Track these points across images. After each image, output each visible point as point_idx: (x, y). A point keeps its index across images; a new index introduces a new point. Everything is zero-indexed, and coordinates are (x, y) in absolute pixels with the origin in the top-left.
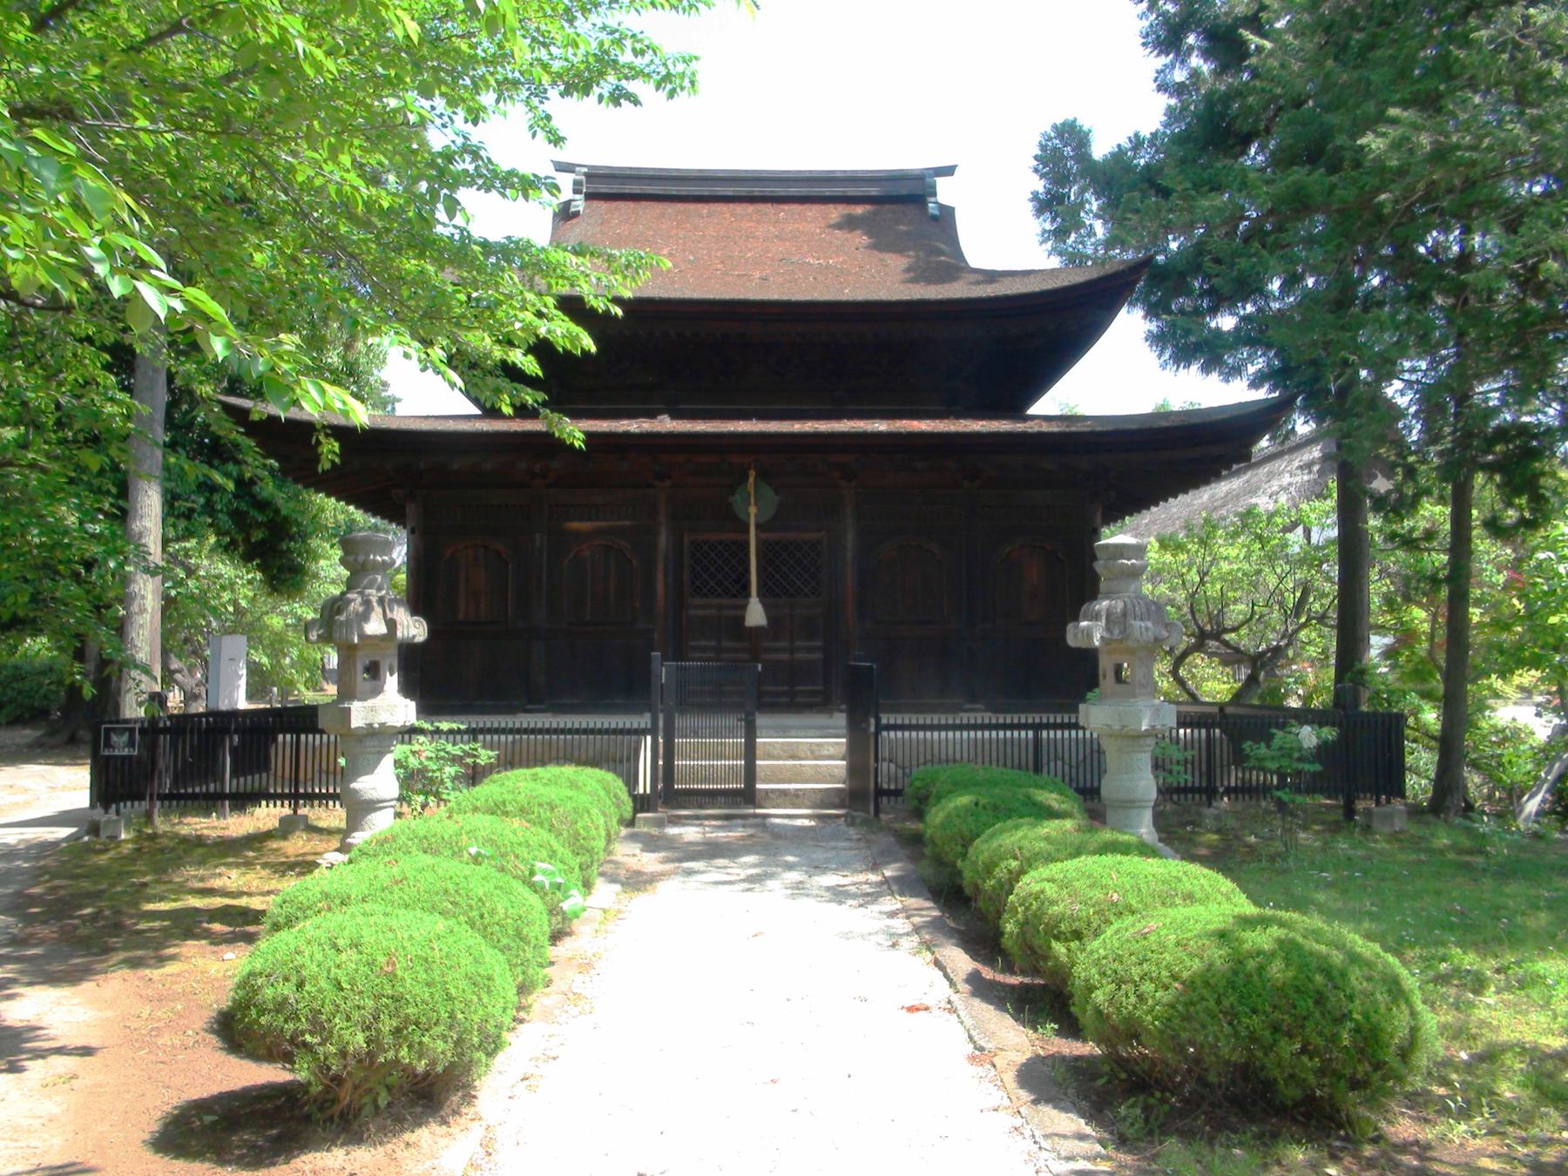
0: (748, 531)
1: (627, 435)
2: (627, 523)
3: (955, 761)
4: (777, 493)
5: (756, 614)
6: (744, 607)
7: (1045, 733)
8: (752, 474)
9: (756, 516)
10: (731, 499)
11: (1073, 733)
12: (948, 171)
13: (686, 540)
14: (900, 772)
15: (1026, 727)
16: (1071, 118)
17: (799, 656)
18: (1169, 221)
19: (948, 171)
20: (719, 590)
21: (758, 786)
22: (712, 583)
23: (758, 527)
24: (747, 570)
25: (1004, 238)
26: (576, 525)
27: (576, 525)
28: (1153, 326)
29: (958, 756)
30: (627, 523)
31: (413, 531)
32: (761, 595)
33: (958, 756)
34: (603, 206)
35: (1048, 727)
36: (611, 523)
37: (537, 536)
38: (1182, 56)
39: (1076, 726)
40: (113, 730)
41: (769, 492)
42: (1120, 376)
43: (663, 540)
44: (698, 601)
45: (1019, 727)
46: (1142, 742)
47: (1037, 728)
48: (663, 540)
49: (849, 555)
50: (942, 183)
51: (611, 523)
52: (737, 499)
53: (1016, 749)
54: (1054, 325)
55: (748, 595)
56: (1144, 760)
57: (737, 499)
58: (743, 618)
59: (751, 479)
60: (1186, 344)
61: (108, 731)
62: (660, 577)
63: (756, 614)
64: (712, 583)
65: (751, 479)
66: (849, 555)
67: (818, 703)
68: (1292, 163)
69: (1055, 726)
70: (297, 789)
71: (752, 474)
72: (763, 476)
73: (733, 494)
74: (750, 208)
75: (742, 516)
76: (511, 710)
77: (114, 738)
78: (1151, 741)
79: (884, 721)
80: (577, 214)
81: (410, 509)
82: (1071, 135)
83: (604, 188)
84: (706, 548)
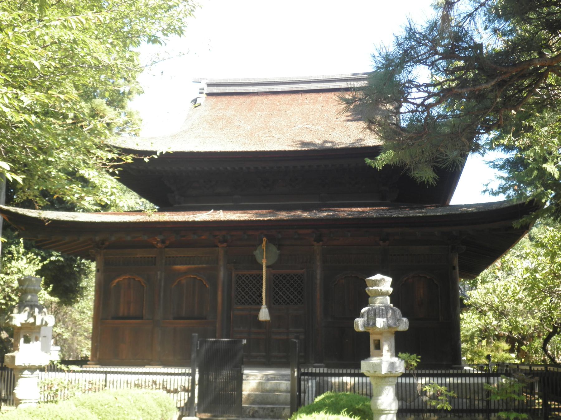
2: (204, 265)
4: (278, 249)
5: (264, 314)
6: (259, 310)
8: (265, 239)
9: (266, 263)
10: (255, 253)
11: (360, 379)
13: (233, 275)
21: (243, 405)
23: (267, 267)
30: (204, 265)
34: (213, 99)
37: (159, 273)
38: (70, 204)
43: (222, 274)
44: (240, 307)
47: (106, 373)
48: (222, 274)
49: (318, 282)
52: (257, 253)
53: (368, 388)
55: (261, 303)
57: (257, 253)
59: (264, 243)
62: (220, 293)
63: (264, 314)
65: (264, 243)
66: (318, 282)
71: (265, 239)
75: (259, 260)
76: (143, 365)
79: (302, 370)
81: (98, 258)
83: (215, 90)
84: (243, 278)
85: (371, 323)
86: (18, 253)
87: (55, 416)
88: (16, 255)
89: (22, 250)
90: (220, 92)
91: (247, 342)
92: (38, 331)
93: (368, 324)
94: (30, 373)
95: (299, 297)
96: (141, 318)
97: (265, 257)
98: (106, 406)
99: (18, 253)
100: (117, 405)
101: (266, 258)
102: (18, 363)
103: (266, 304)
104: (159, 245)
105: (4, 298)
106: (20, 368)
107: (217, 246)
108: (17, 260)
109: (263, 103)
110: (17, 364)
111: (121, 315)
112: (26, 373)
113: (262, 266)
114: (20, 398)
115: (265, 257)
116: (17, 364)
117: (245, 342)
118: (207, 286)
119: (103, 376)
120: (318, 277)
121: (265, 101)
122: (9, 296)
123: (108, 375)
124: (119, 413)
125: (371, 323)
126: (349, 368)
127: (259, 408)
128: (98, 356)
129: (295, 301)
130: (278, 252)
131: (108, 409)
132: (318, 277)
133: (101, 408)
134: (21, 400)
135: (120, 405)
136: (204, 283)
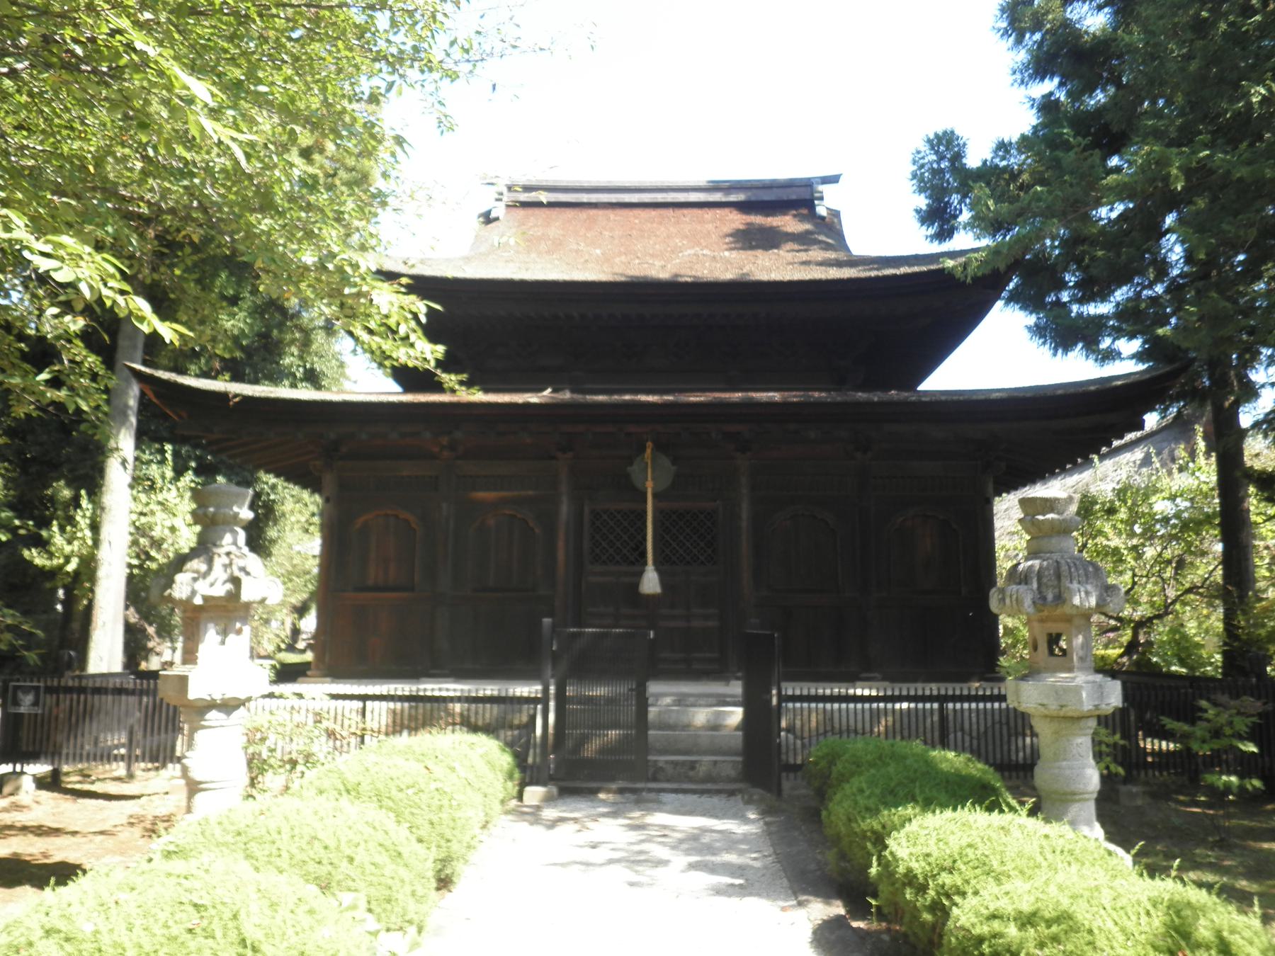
0: (645, 502)
1: (527, 405)
2: (531, 493)
3: (856, 732)
4: (673, 464)
5: (651, 582)
6: (640, 574)
7: (951, 705)
8: (649, 444)
12: (834, 179)
13: (587, 510)
14: (799, 742)
15: (931, 699)
16: (949, 129)
17: (696, 624)
18: (1037, 221)
19: (834, 179)
20: (618, 558)
22: (611, 551)
23: (655, 496)
24: (645, 539)
25: (884, 225)
26: (481, 495)
27: (481, 495)
28: (1032, 319)
29: (860, 726)
30: (531, 493)
31: (327, 500)
32: (657, 563)
33: (860, 726)
34: (521, 212)
35: (954, 699)
36: (516, 493)
37: (444, 505)
39: (1002, 698)
40: (19, 687)
41: (666, 462)
42: (1000, 355)
43: (565, 509)
45: (924, 699)
46: (1082, 723)
47: (364, 698)
48: (565, 509)
49: (744, 524)
50: (825, 189)
51: (516, 493)
52: (634, 470)
54: (937, 306)
55: (645, 563)
56: (1082, 744)
57: (634, 470)
58: (636, 585)
59: (649, 451)
60: (1064, 333)
61: (16, 688)
62: (561, 544)
63: (651, 582)
64: (611, 551)
66: (744, 524)
67: (717, 672)
68: (820, 822)
69: (961, 699)
70: (122, 758)
71: (649, 444)
72: (660, 447)
73: (631, 464)
74: (653, 213)
77: (20, 695)
78: (1093, 723)
80: (497, 219)
81: (328, 479)
82: (946, 144)
85: (1050, 597)
86: (163, 477)
87: (307, 838)
88: (159, 483)
89: (169, 474)
90: (534, 202)
91: (655, 634)
92: (242, 614)
93: (1044, 598)
94: (222, 716)
95: (710, 551)
96: (412, 589)
97: (651, 478)
98: (410, 791)
99: (163, 477)
100: (433, 786)
101: (653, 479)
102: (194, 693)
103: (655, 563)
104: (446, 453)
105: (138, 556)
106: (200, 704)
107: (553, 458)
108: (161, 490)
109: (608, 220)
110: (192, 695)
111: (370, 582)
112: (213, 716)
113: (645, 494)
114: (198, 779)
115: (651, 478)
116: (192, 695)
117: (652, 634)
118: (537, 530)
119: (358, 704)
120: (745, 515)
121: (612, 216)
122: (147, 554)
123: (369, 703)
124: (441, 807)
125: (1050, 597)
126: (821, 684)
127: (667, 762)
128: (327, 659)
129: (702, 558)
130: (674, 468)
131: (416, 798)
132: (745, 515)
133: (401, 795)
134: (201, 783)
135: (439, 785)
136: (531, 524)
